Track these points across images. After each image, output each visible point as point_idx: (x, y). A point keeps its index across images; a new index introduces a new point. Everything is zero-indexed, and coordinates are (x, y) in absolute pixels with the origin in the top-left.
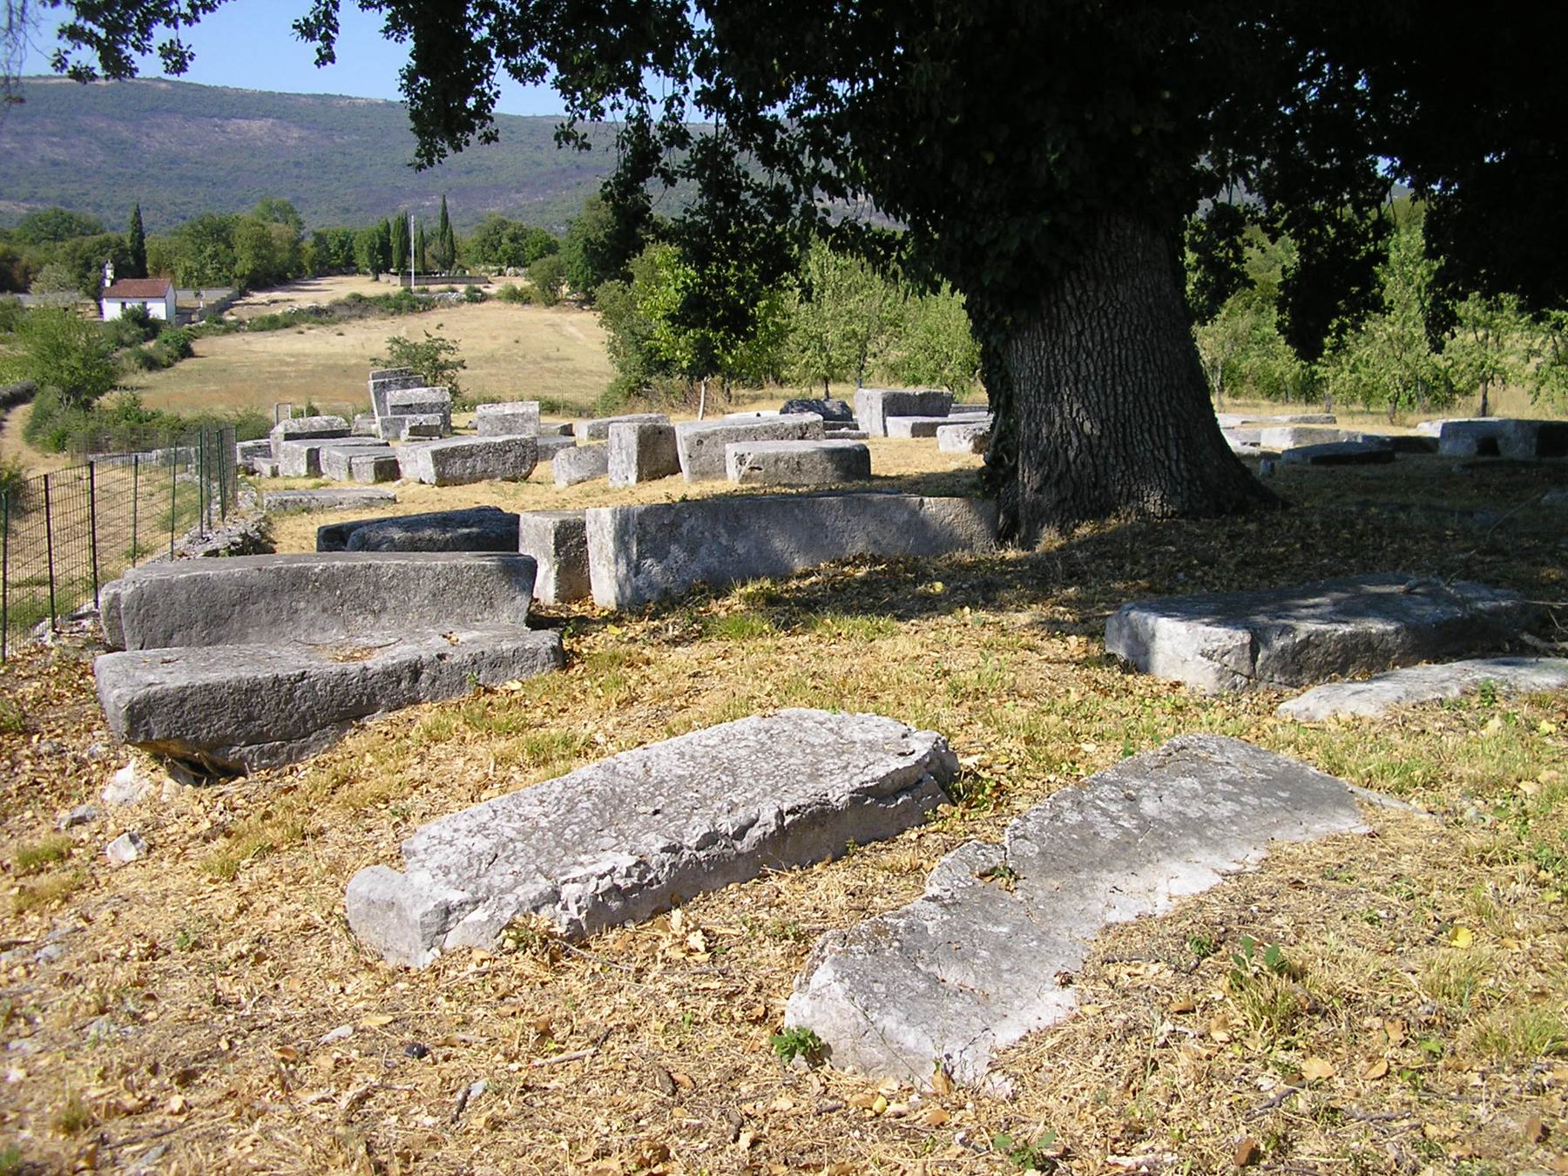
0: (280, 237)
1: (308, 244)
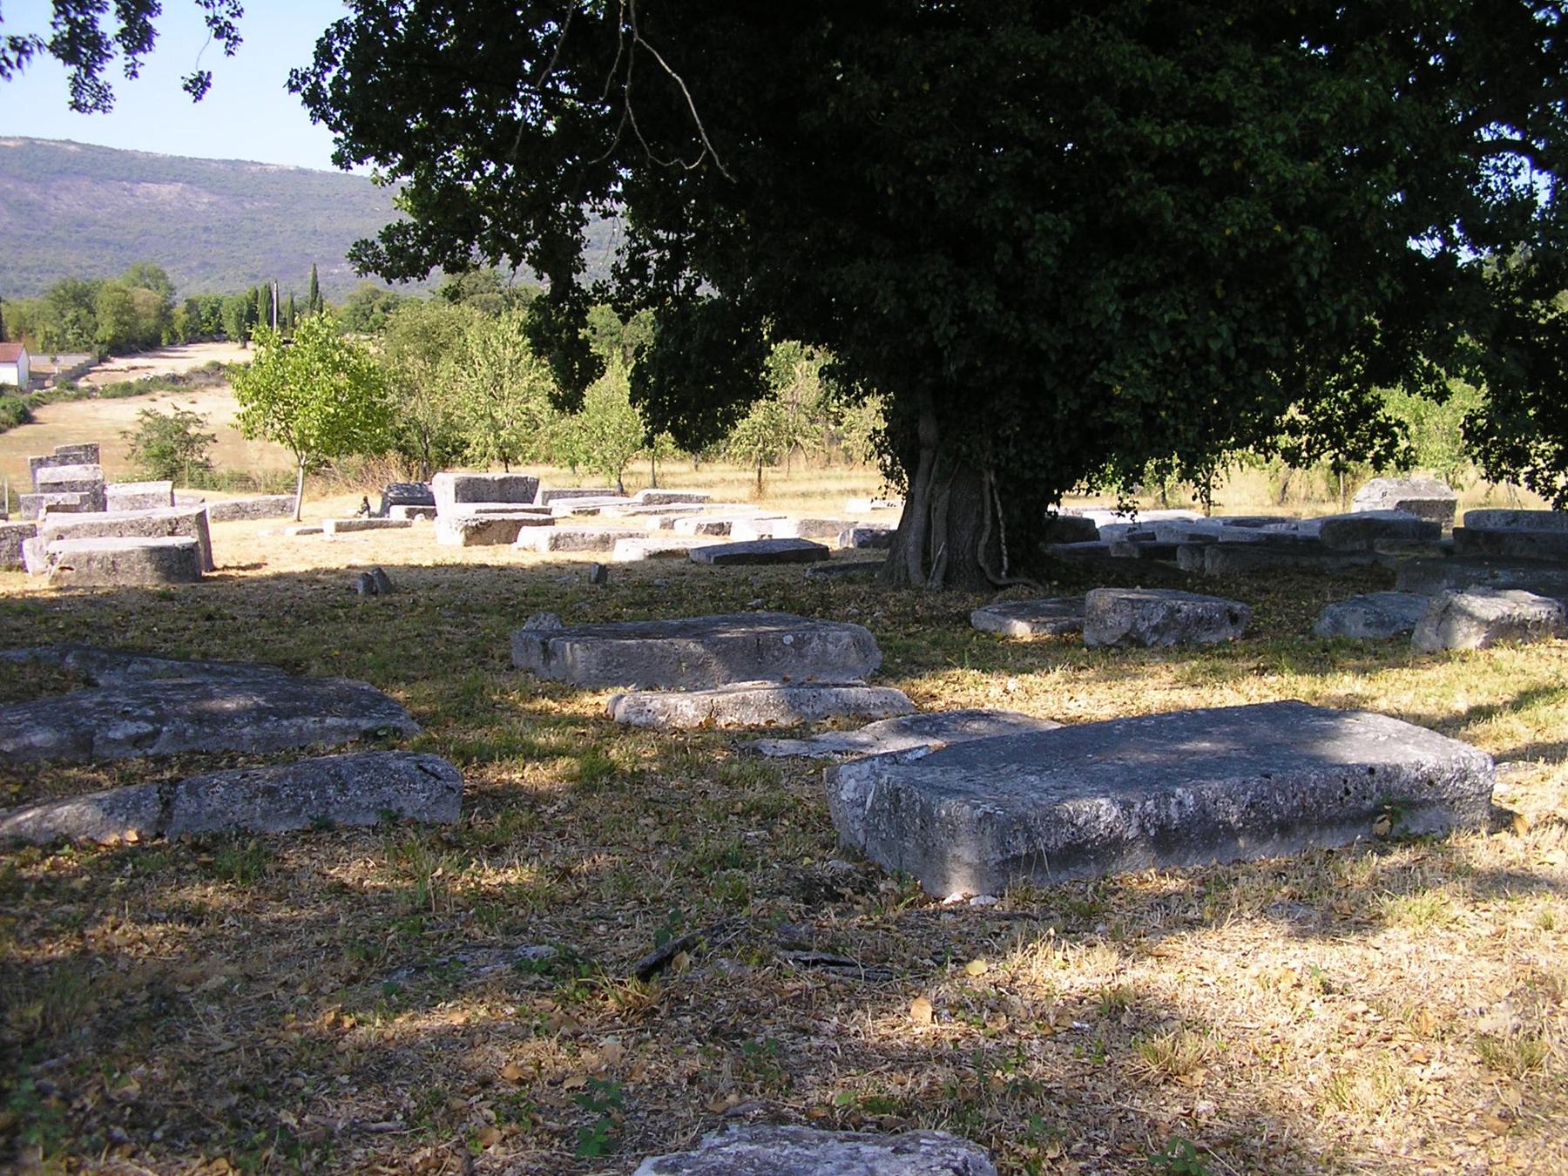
0: (146, 302)
1: (179, 310)
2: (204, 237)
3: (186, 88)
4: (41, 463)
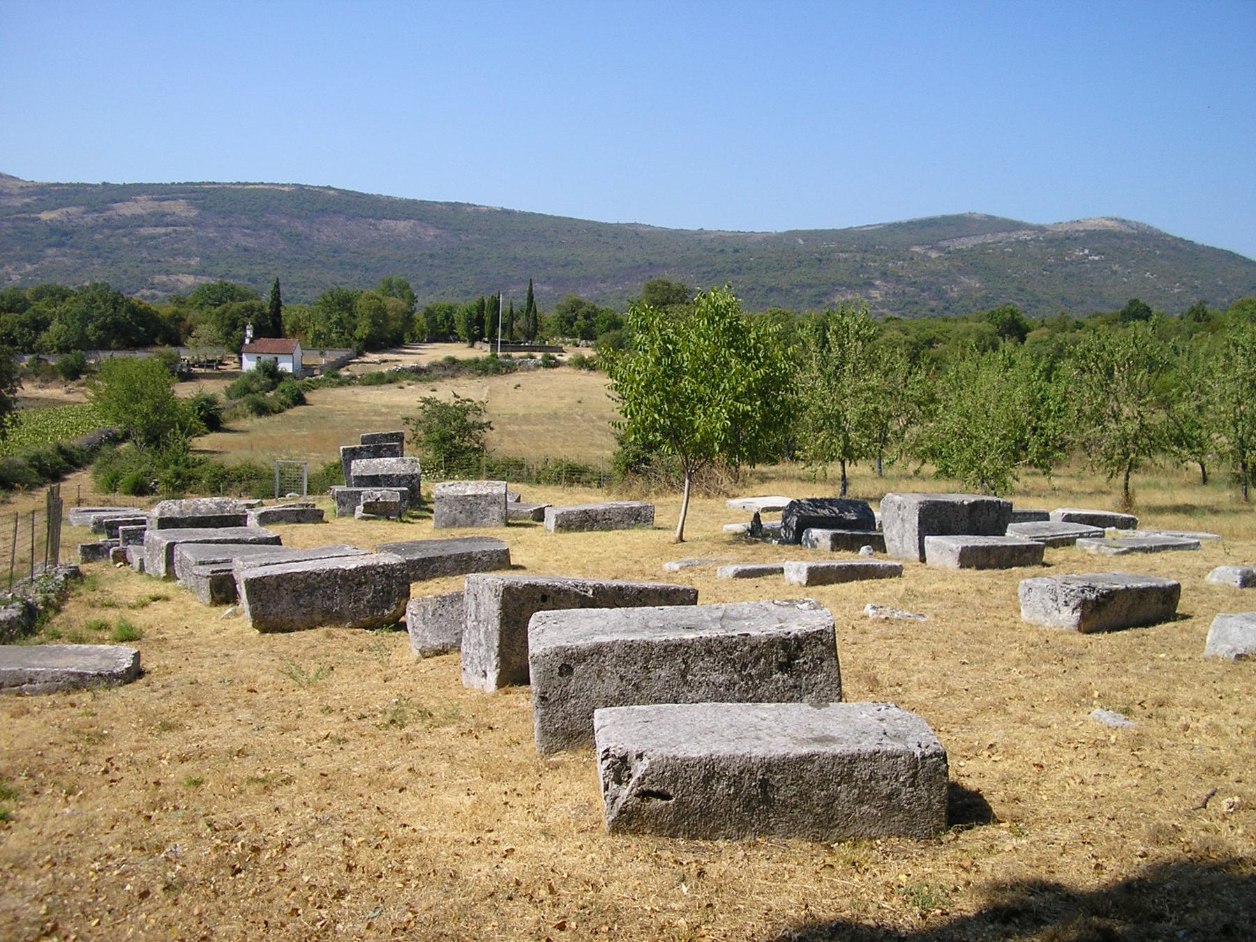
0: (395, 309)
1: (419, 315)
2: (430, 261)
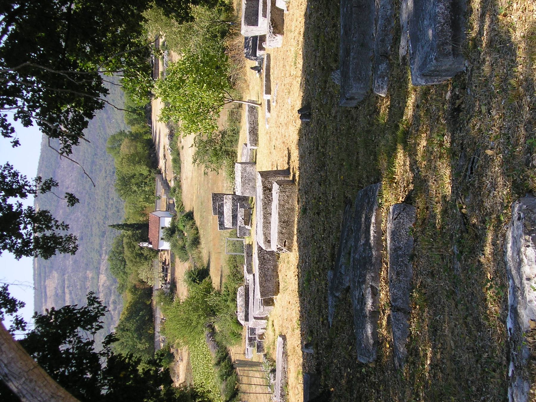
0: (129, 147)
1: (134, 129)
3: (72, 205)
4: (222, 224)
